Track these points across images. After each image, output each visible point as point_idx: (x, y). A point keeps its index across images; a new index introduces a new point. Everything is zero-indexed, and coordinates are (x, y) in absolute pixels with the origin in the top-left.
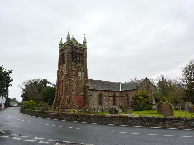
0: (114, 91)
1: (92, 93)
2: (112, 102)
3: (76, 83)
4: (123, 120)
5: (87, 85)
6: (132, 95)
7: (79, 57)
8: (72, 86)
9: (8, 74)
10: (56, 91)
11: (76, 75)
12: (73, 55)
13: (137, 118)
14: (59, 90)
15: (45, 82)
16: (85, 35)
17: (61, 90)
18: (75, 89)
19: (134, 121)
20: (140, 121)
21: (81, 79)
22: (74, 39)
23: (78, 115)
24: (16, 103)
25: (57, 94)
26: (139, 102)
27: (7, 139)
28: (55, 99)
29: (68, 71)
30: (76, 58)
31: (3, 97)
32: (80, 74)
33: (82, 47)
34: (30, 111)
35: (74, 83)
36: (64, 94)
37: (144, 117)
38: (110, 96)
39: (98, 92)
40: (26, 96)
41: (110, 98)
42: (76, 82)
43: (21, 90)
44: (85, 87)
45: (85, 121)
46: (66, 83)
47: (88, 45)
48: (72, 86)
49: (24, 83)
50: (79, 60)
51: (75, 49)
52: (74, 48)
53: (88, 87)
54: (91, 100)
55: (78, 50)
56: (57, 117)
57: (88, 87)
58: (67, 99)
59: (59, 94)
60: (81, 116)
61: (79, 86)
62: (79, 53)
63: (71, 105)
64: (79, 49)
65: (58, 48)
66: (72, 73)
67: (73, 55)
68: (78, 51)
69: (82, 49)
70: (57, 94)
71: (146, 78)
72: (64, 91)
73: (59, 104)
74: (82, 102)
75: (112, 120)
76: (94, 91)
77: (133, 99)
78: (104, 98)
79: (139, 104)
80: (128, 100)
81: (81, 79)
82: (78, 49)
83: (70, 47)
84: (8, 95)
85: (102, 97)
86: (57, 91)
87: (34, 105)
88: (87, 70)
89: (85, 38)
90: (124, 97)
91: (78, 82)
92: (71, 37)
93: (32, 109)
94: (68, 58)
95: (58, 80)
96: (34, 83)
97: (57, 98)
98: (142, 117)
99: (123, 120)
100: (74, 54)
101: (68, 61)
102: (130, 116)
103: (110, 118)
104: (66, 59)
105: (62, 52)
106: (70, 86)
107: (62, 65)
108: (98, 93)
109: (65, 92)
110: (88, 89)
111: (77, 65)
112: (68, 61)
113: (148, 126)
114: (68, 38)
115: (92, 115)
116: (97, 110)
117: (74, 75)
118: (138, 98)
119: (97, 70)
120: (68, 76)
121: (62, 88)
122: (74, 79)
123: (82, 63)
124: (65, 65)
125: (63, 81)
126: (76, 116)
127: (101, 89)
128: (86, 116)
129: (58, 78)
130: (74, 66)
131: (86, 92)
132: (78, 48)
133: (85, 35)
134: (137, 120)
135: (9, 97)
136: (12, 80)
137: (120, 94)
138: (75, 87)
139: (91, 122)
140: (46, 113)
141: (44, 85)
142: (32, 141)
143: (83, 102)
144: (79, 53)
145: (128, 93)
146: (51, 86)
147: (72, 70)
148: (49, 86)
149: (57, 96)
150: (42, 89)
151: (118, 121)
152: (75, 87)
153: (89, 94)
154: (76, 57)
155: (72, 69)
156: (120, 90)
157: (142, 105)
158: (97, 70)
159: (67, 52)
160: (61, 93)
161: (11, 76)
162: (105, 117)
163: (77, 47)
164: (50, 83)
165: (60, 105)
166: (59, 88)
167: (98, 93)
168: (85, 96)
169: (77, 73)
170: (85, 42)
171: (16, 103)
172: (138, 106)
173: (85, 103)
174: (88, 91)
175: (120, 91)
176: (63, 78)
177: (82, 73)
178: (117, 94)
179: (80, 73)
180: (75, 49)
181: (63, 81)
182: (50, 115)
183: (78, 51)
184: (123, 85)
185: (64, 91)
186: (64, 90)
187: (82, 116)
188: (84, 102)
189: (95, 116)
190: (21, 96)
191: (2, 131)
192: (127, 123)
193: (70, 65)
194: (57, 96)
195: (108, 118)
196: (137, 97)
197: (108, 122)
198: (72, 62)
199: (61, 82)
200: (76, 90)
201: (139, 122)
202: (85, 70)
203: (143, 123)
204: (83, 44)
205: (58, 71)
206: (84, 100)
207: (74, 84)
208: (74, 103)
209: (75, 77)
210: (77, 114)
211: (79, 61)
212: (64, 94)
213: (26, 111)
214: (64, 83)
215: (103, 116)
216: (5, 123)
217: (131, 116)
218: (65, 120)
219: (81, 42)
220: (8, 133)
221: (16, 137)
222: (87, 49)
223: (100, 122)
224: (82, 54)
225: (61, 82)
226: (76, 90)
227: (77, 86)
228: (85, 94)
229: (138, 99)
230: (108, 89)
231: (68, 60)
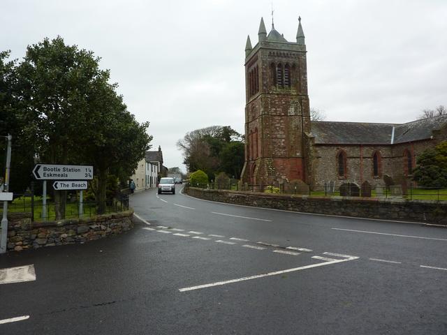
0: (375, 146)
1: (320, 152)
2: (370, 170)
4: (368, 207)
5: (310, 135)
6: (419, 151)
7: (289, 73)
8: (276, 138)
9: (143, 128)
10: (246, 152)
12: (276, 70)
13: (398, 205)
14: (250, 149)
15: (227, 132)
16: (300, 19)
17: (255, 148)
18: (282, 144)
19: (393, 210)
20: (407, 210)
21: (296, 122)
22: (274, 33)
23: (278, 197)
24: (179, 175)
25: (248, 157)
26: (436, 169)
27: (151, 232)
28: (245, 167)
29: (266, 107)
30: (282, 76)
31: (153, 166)
32: (292, 111)
33: (294, 49)
34: (197, 190)
35: (280, 132)
36: (260, 156)
37: (415, 201)
39: (335, 149)
40: (192, 163)
41: (364, 161)
43: (183, 151)
44: (305, 140)
45: (291, 209)
46: (263, 134)
47: (308, 42)
48: (276, 138)
49: (187, 137)
50: (290, 80)
52: (276, 54)
53: (311, 138)
56: (241, 201)
57: (312, 139)
58: (268, 165)
59: (251, 157)
60: (284, 200)
62: (287, 65)
63: (277, 178)
65: (242, 58)
66: (276, 111)
67: (276, 70)
68: (284, 60)
69: (294, 55)
70: (248, 157)
72: (260, 151)
73: (253, 177)
74: (299, 173)
75: (345, 208)
77: (419, 162)
78: (350, 161)
79: (436, 174)
80: (410, 165)
81: (294, 123)
82: (286, 56)
83: (268, 52)
84: (162, 162)
85: (346, 160)
86: (248, 151)
87: (205, 179)
89: (300, 26)
90: (402, 159)
91: (287, 130)
92: (268, 30)
93: (201, 186)
94: (263, 79)
95: (248, 127)
96: (206, 136)
97: (247, 164)
98: (410, 201)
99: (368, 207)
100: (277, 69)
101: (264, 85)
102: (382, 200)
103: (340, 203)
104: (260, 81)
105: (252, 67)
106: (272, 138)
107: (253, 95)
108: (335, 151)
109: (262, 152)
110: (311, 143)
111: (283, 92)
112: (264, 85)
113: (425, 221)
114: (262, 32)
115: (304, 196)
116: (332, 187)
117: (280, 116)
118: (434, 160)
119: (333, 98)
120: (267, 118)
121: (257, 144)
122: (279, 124)
123: (295, 86)
124: (259, 95)
125: (256, 130)
126: (275, 199)
127: (342, 143)
128: (294, 200)
129: (247, 124)
130: (278, 95)
131: (308, 149)
132: (285, 52)
133: (300, 19)
134: (400, 208)
135: (163, 164)
136: (151, 138)
137: (392, 152)
138: (283, 140)
139: (302, 210)
140: (222, 193)
141: (224, 139)
142: (184, 235)
143: (301, 171)
144: (287, 65)
145: (410, 148)
146: (240, 139)
147: (273, 105)
148: (235, 140)
149: (248, 161)
150: (221, 147)
151: (358, 209)
152: (283, 140)
153: (313, 154)
154: (282, 73)
156: (392, 143)
157: (442, 176)
158: (333, 98)
159: (260, 66)
160: (255, 155)
161: (148, 132)
162: (331, 202)
163: (282, 52)
164: (238, 134)
165: (255, 178)
166: (251, 144)
167: (335, 151)
168: (305, 158)
169: (286, 110)
170: (301, 36)
171: (179, 175)
172: (432, 178)
173: (306, 174)
174: (311, 148)
175: (391, 145)
176: (257, 124)
177: (296, 109)
178: (383, 152)
179: (293, 109)
181: (256, 130)
182: (230, 197)
184: (401, 129)
185: (260, 151)
186: (260, 148)
187: (284, 199)
188: (304, 170)
189: (309, 200)
190: (185, 163)
191: (145, 222)
192: (377, 215)
194: (248, 161)
195: (336, 204)
196: (429, 157)
197: (337, 212)
198: (273, 87)
199: (254, 130)
200: (284, 148)
201: (402, 213)
203: (413, 215)
204: (295, 41)
205: (247, 109)
206: (304, 167)
207: (280, 134)
208: (282, 173)
210: (277, 195)
211: (289, 81)
212: (260, 156)
213: (192, 189)
214: (260, 133)
215: (327, 199)
216: (153, 210)
217: (387, 200)
218: (255, 206)
219: (291, 38)
220: (154, 224)
221: (164, 230)
222: (306, 52)
223: (320, 211)
224: (294, 66)
225: (254, 130)
226: (284, 148)
227: (287, 139)
228: (305, 156)
229: (434, 161)
230: (359, 141)
231: (265, 83)
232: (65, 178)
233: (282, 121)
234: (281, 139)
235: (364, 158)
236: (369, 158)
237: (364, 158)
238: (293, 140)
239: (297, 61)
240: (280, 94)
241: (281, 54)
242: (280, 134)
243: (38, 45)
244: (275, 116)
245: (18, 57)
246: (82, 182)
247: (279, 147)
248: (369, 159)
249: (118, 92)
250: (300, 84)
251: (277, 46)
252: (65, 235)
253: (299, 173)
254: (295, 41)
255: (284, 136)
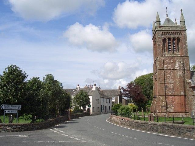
16: (181, 11)
35: (171, 80)
62: (174, 39)
66: (167, 67)
69: (178, 32)
89: (182, 15)
111: (171, 54)
133: (181, 11)
138: (173, 85)
152: (173, 85)
177: (179, 65)
179: (178, 65)
224: (179, 39)
232: (11, 109)
233: (171, 73)
234: (171, 84)
243: (5, 71)
245: (2, 74)
246: (15, 111)
252: (8, 129)
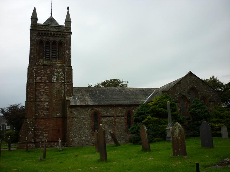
2: (42, 156)
3: (47, 95)
11: (47, 81)
16: (68, 8)
18: (46, 106)
28: (150, 96)
32: (54, 78)
35: (45, 96)
38: (119, 115)
39: (90, 109)
42: (48, 94)
44: (65, 103)
48: (41, 101)
51: (47, 35)
54: (73, 125)
55: (52, 36)
61: (54, 101)
64: (54, 34)
66: (41, 79)
69: (60, 34)
71: (190, 74)
74: (59, 130)
76: (81, 109)
81: (56, 89)
88: (72, 70)
89: (68, 13)
92: (42, 20)
108: (90, 111)
130: (43, 66)
132: (52, 33)
133: (68, 8)
136: (213, 77)
138: (47, 103)
152: (47, 103)
155: (41, 72)
163: (49, 32)
167: (90, 111)
168: (64, 118)
170: (68, 21)
180: (47, 35)
183: (52, 39)
193: (35, 65)
200: (47, 109)
202: (66, 70)
204: (64, 25)
207: (44, 98)
208: (45, 131)
209: (45, 86)
219: (61, 22)
224: (60, 43)
235: (118, 116)
236: (122, 116)
237: (118, 116)
238: (55, 102)
239: (63, 40)
240: (46, 65)
241: (48, 34)
242: (44, 98)
244: (39, 83)
247: (43, 109)
248: (123, 118)
249: (217, 79)
250: (65, 57)
251: (46, 28)
253: (59, 130)
254: (64, 25)
255: (48, 100)
